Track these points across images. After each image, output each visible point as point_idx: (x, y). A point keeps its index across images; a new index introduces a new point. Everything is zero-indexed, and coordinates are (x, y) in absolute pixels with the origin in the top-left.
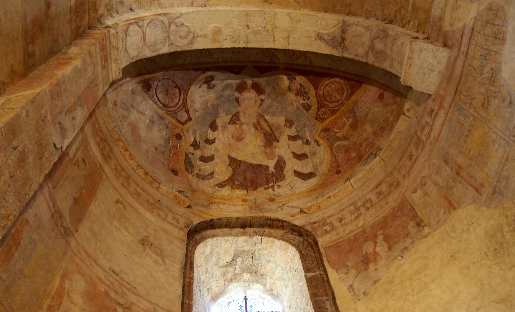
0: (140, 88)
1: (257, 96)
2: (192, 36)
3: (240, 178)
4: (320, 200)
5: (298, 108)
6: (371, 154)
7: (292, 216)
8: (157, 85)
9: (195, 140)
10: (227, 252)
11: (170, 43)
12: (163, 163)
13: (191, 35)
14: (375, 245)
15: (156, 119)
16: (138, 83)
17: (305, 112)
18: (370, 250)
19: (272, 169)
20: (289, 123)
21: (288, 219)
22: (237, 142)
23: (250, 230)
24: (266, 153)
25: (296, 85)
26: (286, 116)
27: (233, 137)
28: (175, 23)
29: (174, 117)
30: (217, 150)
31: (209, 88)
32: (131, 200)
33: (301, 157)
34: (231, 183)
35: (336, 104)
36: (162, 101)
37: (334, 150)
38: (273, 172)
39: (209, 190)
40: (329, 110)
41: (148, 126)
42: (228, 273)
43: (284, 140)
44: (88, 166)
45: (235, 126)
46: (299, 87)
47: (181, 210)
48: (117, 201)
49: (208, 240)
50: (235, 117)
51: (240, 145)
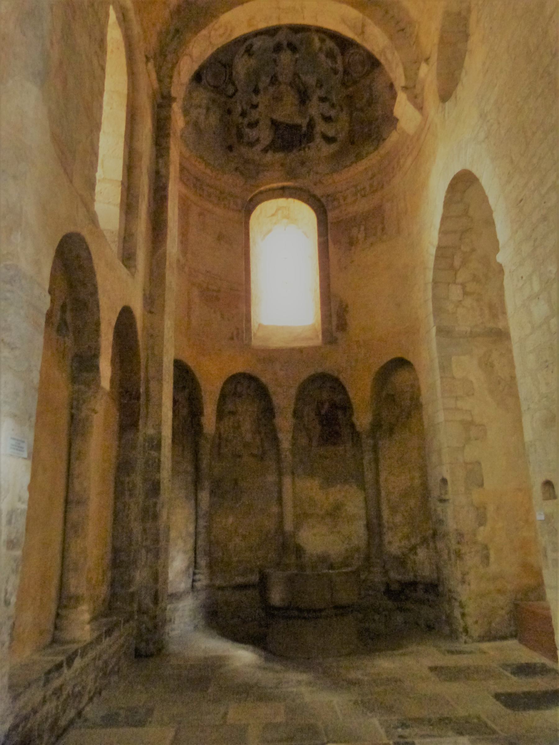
9: (242, 109)
19: (304, 129)
33: (328, 119)
43: (315, 99)
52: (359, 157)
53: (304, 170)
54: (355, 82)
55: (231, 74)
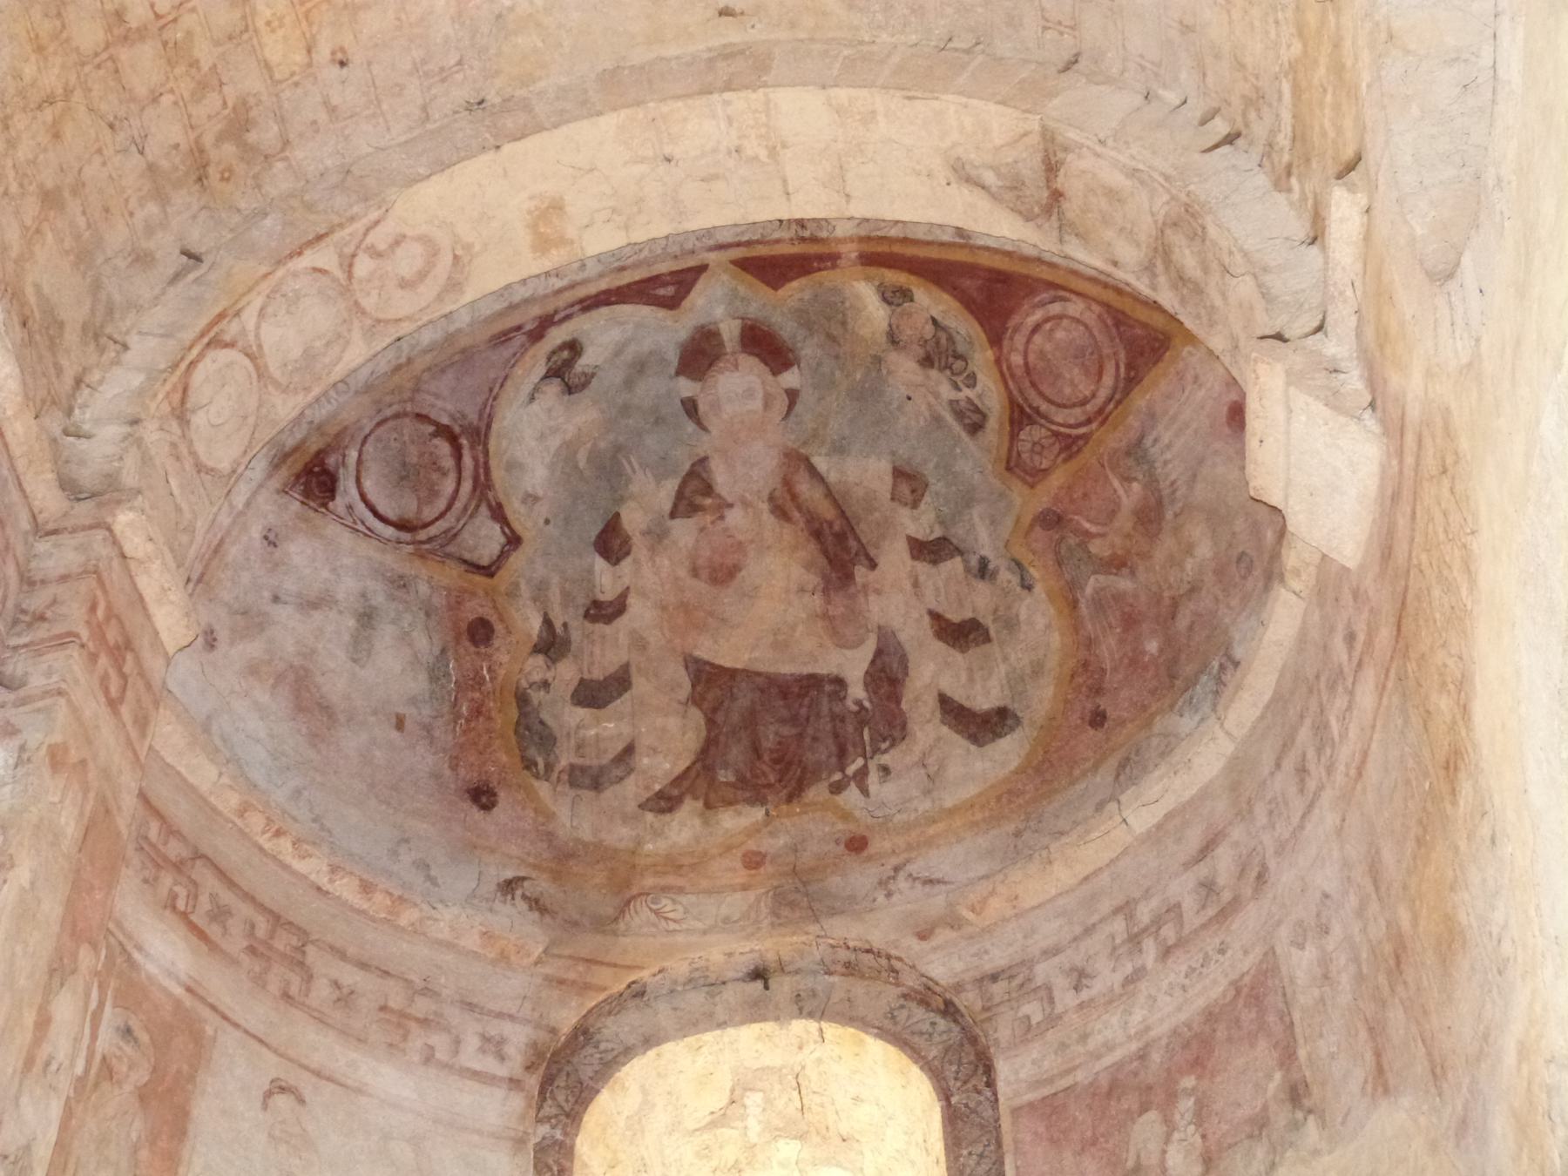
1: (770, 377)
2: (451, 257)
3: (737, 753)
7: (923, 936)
8: (359, 462)
9: (548, 623)
11: (369, 322)
13: (446, 260)
15: (379, 599)
19: (857, 691)
26: (893, 453)
27: (695, 572)
29: (448, 556)
30: (639, 643)
31: (570, 390)
33: (960, 633)
34: (702, 785)
35: (1078, 411)
36: (391, 514)
37: (1084, 609)
38: (859, 703)
39: (620, 835)
40: (1056, 434)
42: (721, 1147)
43: (894, 559)
46: (929, 330)
48: (280, 1088)
50: (694, 484)
52: (1129, 770)
53: (860, 878)
54: (1070, 445)
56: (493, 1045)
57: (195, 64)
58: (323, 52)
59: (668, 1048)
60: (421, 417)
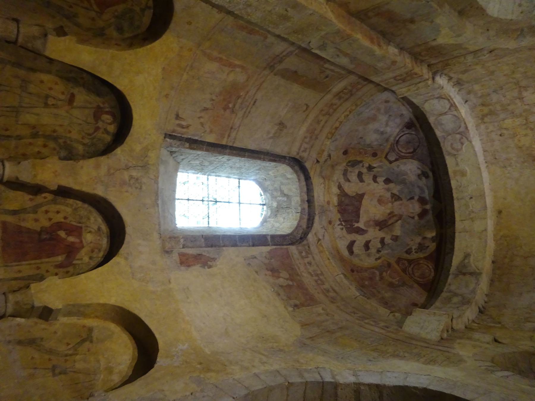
0: (406, 120)
4: (327, 253)
5: (408, 245)
6: (365, 293)
7: (315, 234)
8: (412, 134)
9: (374, 168)
10: (290, 190)
12: (351, 143)
13: (455, 153)
14: (285, 279)
16: (410, 119)
17: (405, 250)
18: (281, 275)
19: (356, 225)
20: (395, 238)
21: (313, 231)
22: (376, 200)
23: (306, 206)
24: (369, 221)
25: (427, 243)
27: (380, 196)
28: (462, 138)
30: (369, 184)
32: (312, 116)
33: (367, 246)
36: (400, 139)
37: (372, 270)
41: (378, 131)
43: (381, 234)
44: (325, 80)
45: (390, 198)
46: (426, 245)
47: (314, 155)
48: (308, 106)
49: (295, 175)
51: (375, 202)
55: (406, 158)
56: (305, 151)
57: (509, 105)
58: (505, 132)
59: (298, 183)
60: (418, 146)
